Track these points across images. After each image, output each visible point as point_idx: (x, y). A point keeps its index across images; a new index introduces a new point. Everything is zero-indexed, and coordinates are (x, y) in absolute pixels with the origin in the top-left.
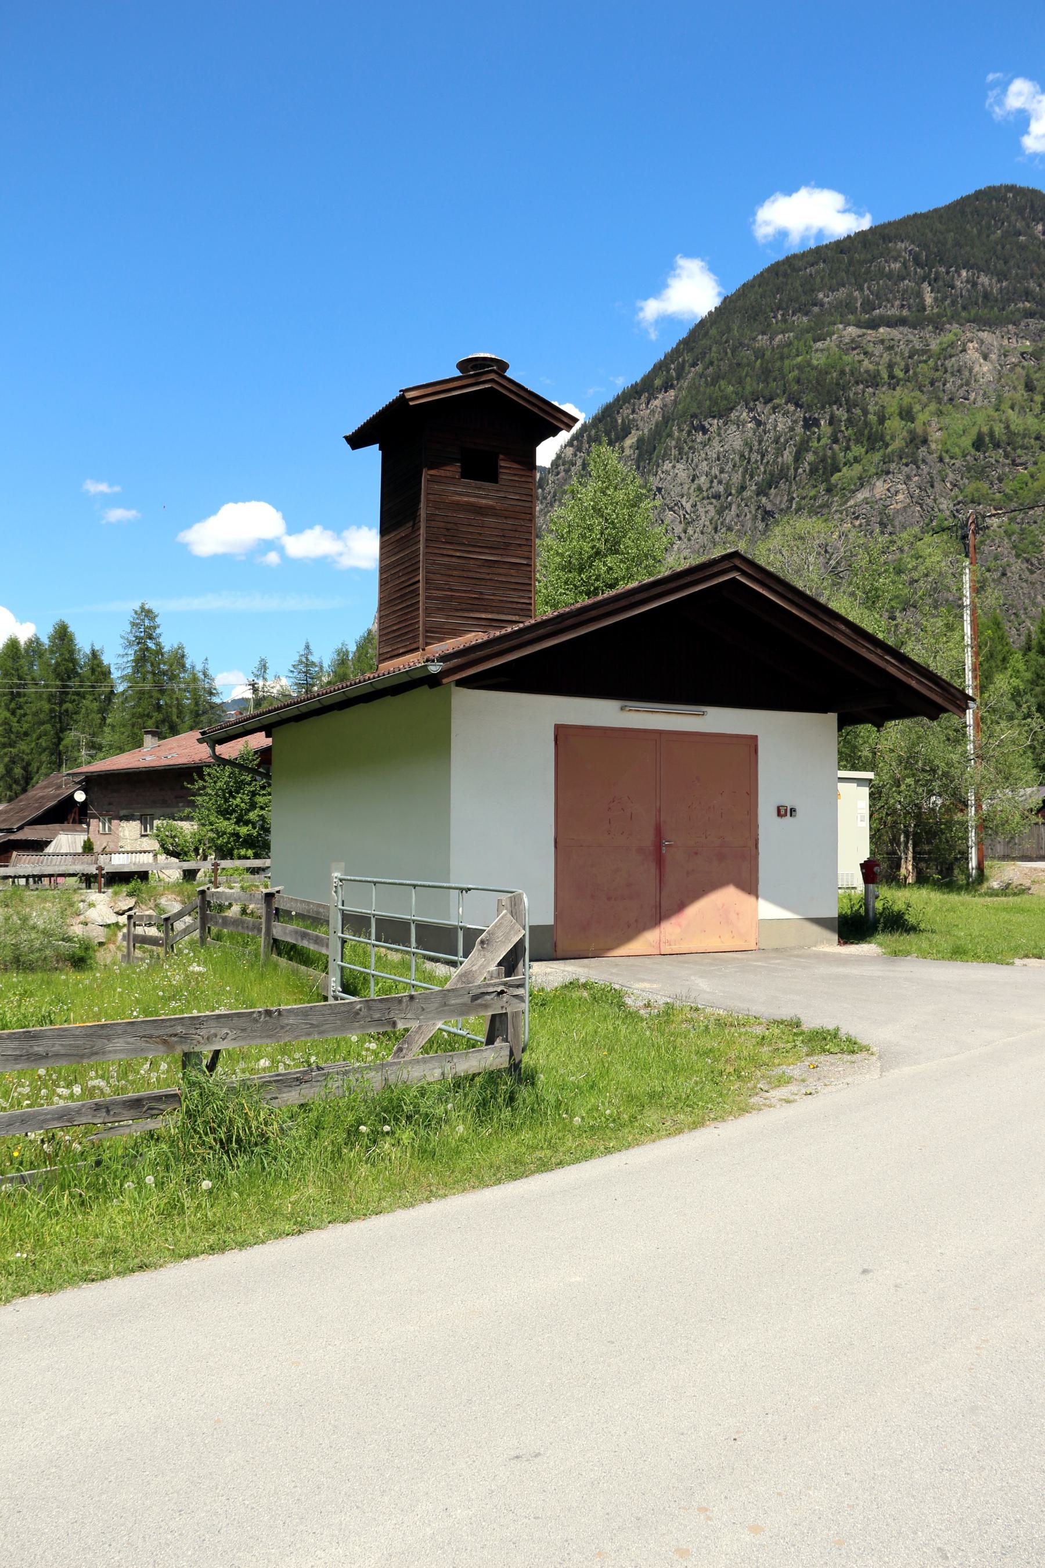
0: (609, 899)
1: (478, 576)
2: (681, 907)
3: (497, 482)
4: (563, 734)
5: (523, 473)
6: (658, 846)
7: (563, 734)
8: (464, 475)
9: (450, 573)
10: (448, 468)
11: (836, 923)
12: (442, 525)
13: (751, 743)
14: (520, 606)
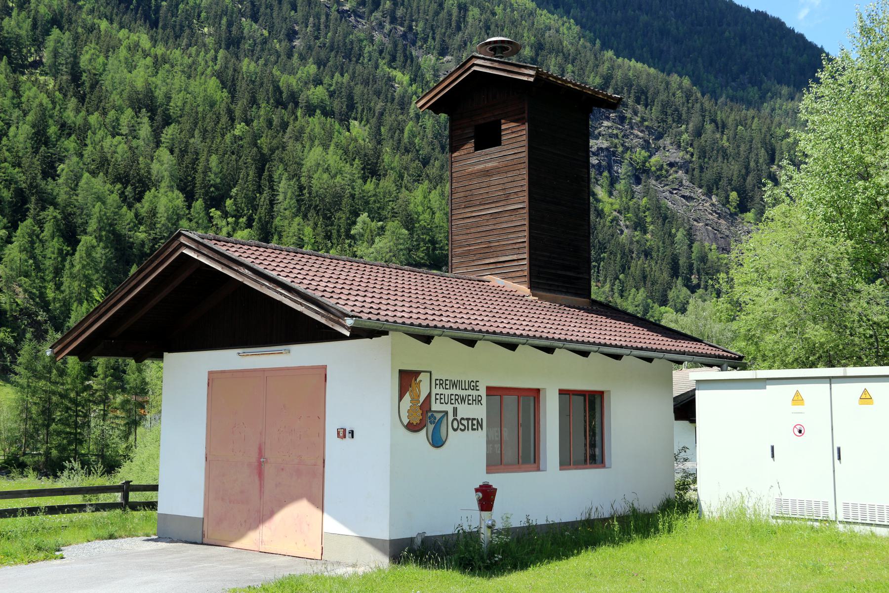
0: (230, 502)
1: (488, 228)
2: (272, 514)
3: (500, 144)
4: (214, 378)
5: (519, 129)
6: (260, 464)
7: (214, 378)
8: (477, 149)
9: (468, 231)
10: (465, 147)
11: (388, 545)
12: (462, 194)
13: (321, 373)
14: (517, 246)
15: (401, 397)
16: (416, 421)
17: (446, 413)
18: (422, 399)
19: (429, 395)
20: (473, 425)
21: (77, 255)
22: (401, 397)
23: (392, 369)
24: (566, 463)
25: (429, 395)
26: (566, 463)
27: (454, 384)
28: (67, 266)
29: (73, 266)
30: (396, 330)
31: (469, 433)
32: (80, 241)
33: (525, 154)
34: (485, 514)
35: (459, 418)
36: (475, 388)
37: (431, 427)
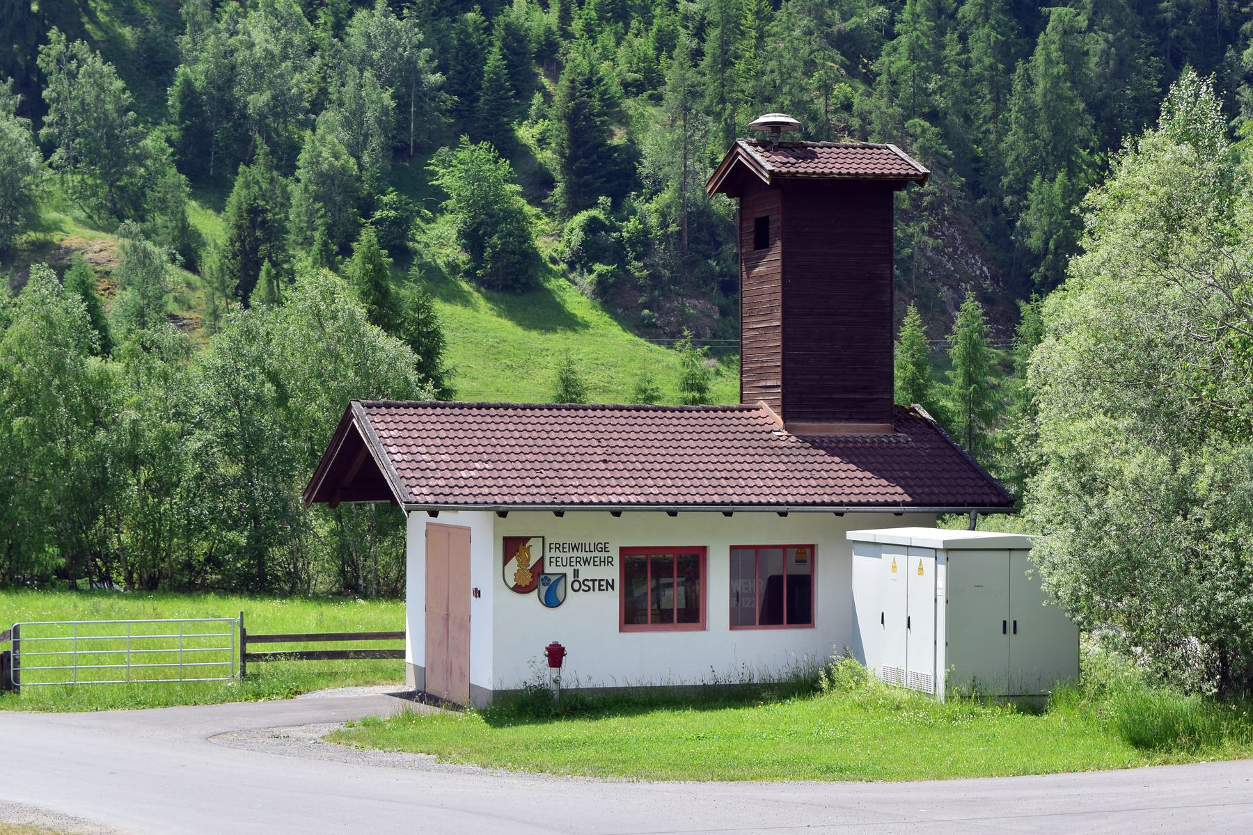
15: (505, 562)
16: (525, 582)
17: (564, 575)
18: (532, 563)
19: (542, 560)
20: (600, 585)
21: (1039, 56)
22: (505, 562)
23: (495, 536)
24: (739, 620)
25: (542, 560)
26: (739, 620)
27: (575, 548)
28: (1018, 86)
29: (1030, 82)
30: (446, 509)
31: (596, 596)
32: (1046, 20)
33: (779, 263)
34: (555, 670)
35: (581, 579)
36: (605, 549)
37: (544, 589)
